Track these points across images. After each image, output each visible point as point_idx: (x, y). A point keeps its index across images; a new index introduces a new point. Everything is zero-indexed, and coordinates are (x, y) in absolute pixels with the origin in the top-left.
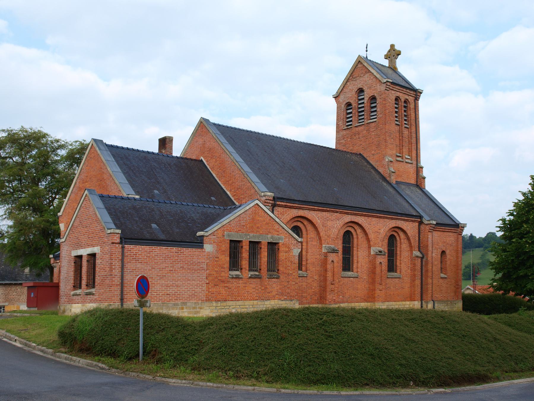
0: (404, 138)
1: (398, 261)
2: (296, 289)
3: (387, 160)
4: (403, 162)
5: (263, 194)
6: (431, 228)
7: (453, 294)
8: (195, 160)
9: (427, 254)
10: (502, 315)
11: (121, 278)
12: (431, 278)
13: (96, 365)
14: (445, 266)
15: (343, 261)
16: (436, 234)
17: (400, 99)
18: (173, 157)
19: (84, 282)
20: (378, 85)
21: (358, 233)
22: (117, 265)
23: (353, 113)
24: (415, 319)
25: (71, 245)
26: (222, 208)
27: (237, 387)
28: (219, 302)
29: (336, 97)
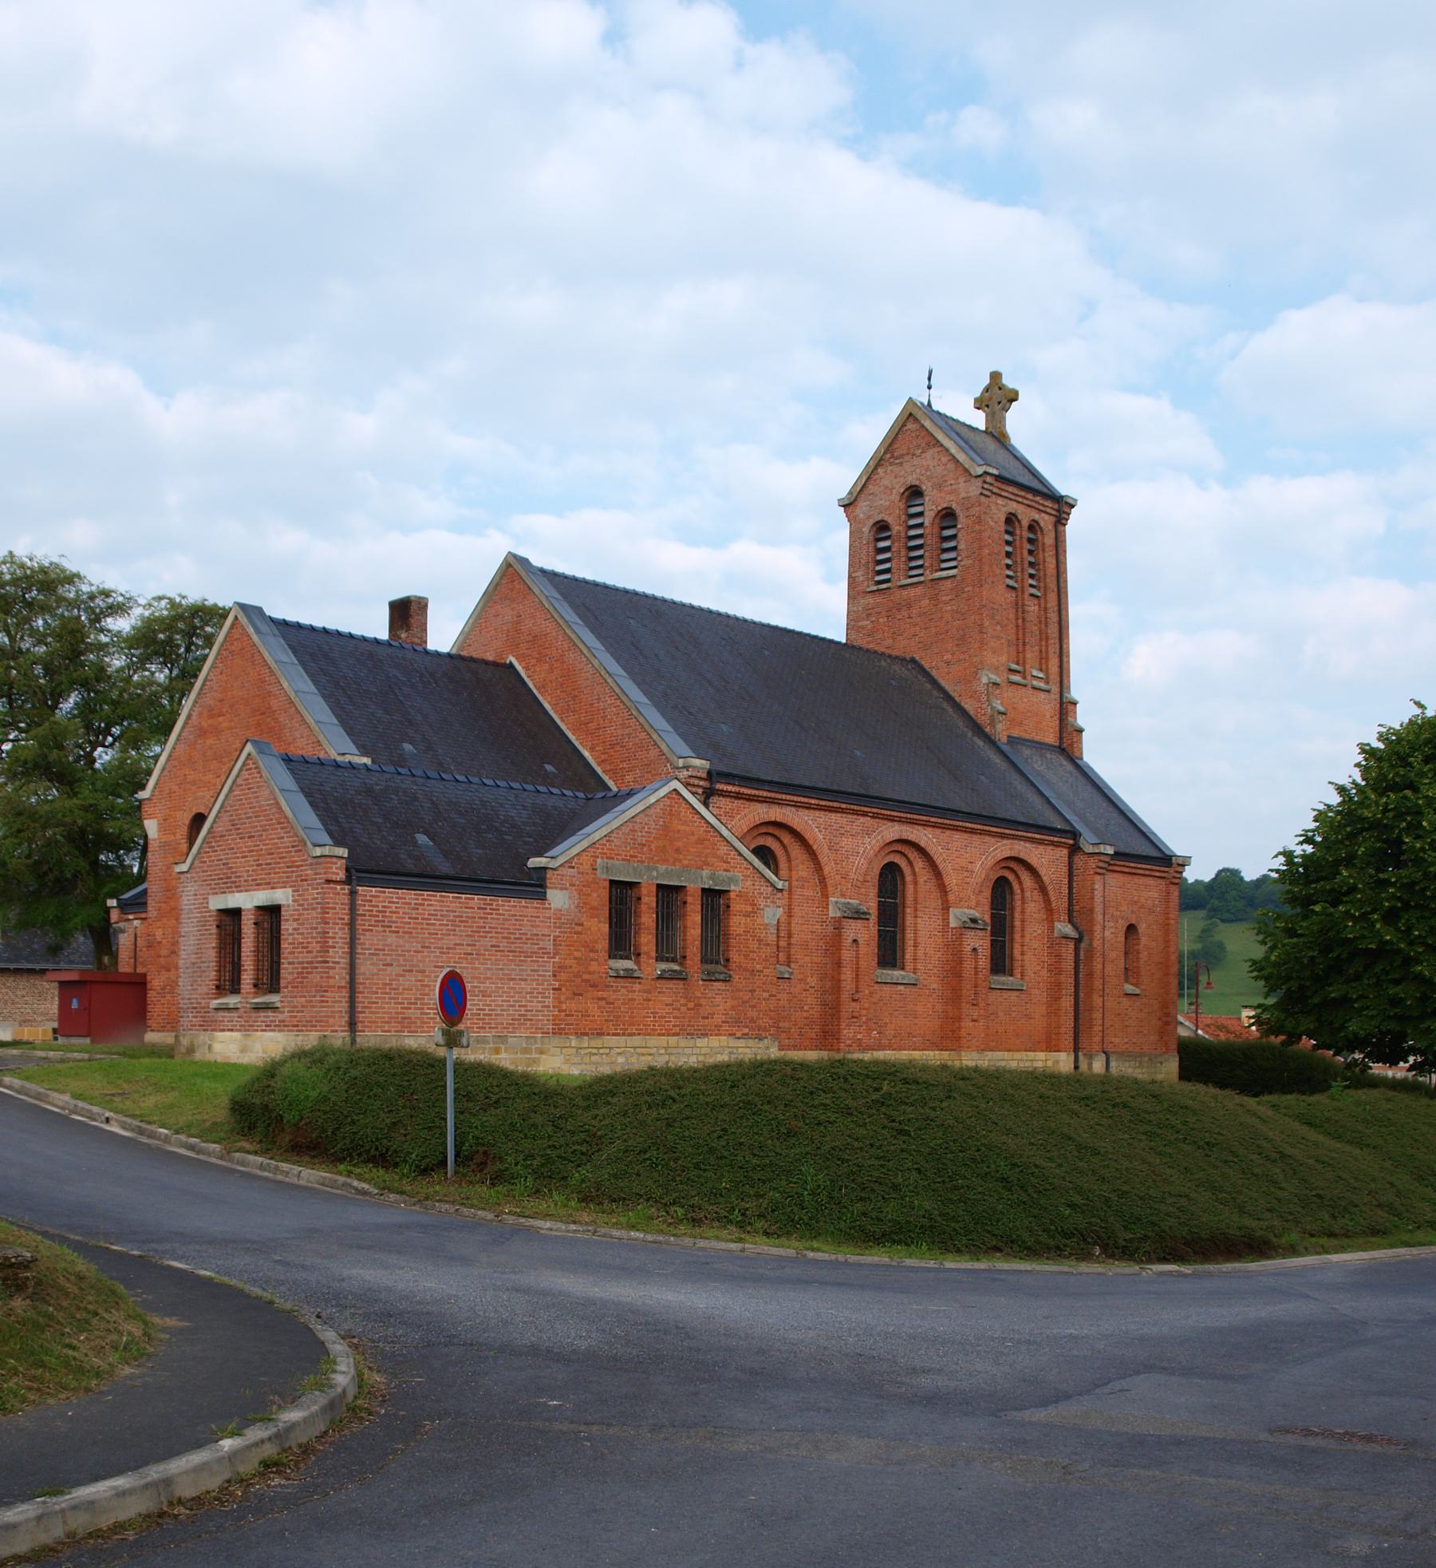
0: (1027, 625)
1: (1017, 946)
2: (771, 1011)
3: (985, 680)
4: (1025, 686)
5: (681, 763)
6: (1101, 864)
7: (1154, 1038)
8: (495, 664)
9: (1092, 932)
10: (1290, 1099)
11: (348, 970)
12: (1101, 993)
13: (344, 1184)
14: (1135, 964)
15: (879, 940)
16: (1113, 880)
17: (1019, 521)
18: (427, 652)
19: (247, 978)
20: (961, 480)
21: (917, 870)
22: (341, 938)
23: (893, 549)
24: (1091, 1097)
25: (206, 880)
26: (581, 795)
27: (701, 1243)
28: (586, 1038)
29: (848, 505)
